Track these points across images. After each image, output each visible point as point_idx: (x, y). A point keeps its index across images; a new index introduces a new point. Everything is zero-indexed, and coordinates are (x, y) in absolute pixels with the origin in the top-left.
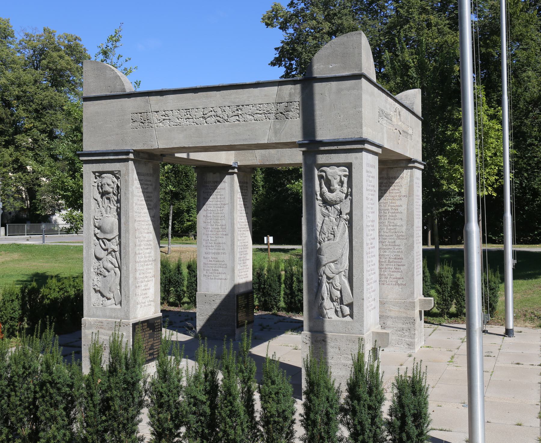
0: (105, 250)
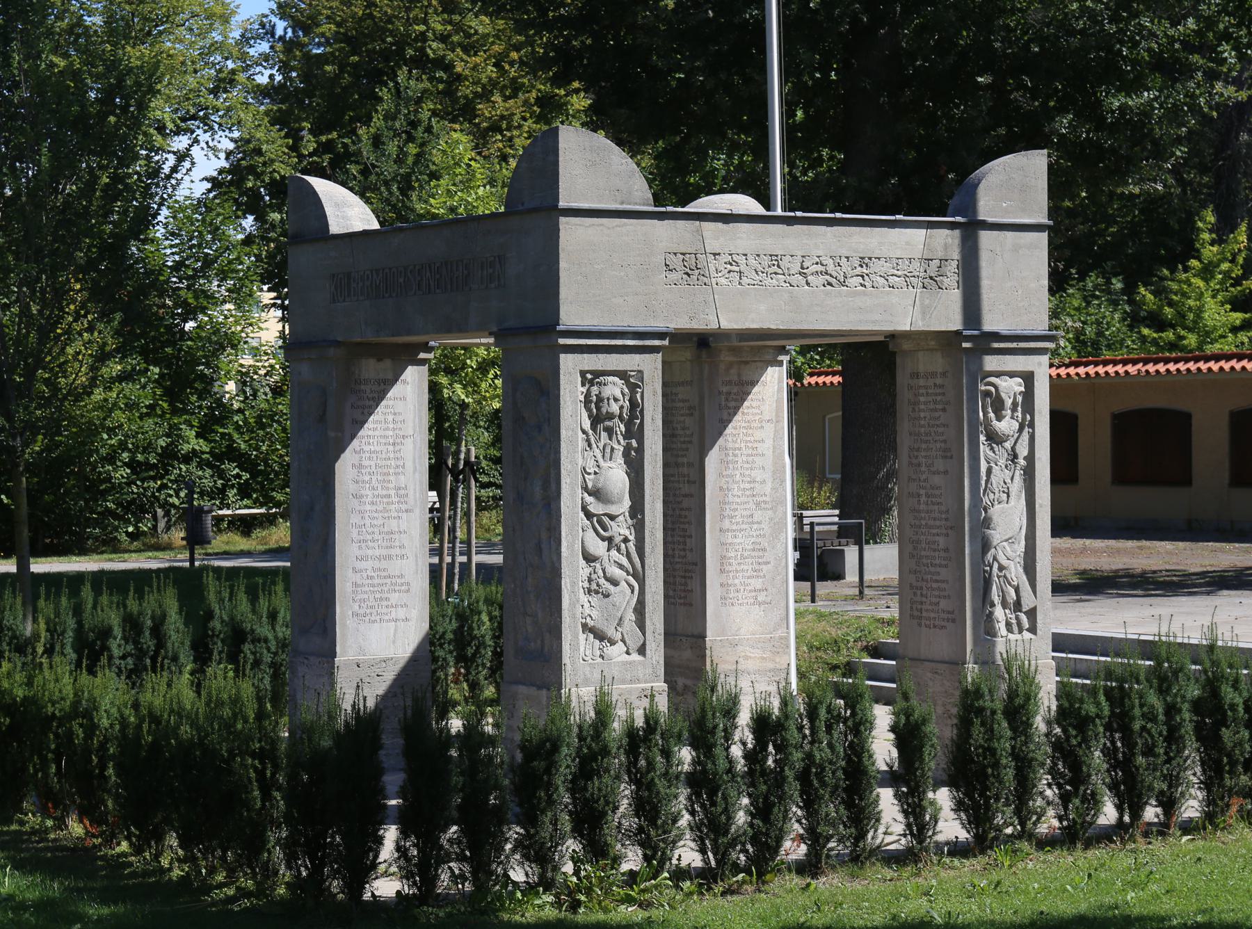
0: (603, 539)
